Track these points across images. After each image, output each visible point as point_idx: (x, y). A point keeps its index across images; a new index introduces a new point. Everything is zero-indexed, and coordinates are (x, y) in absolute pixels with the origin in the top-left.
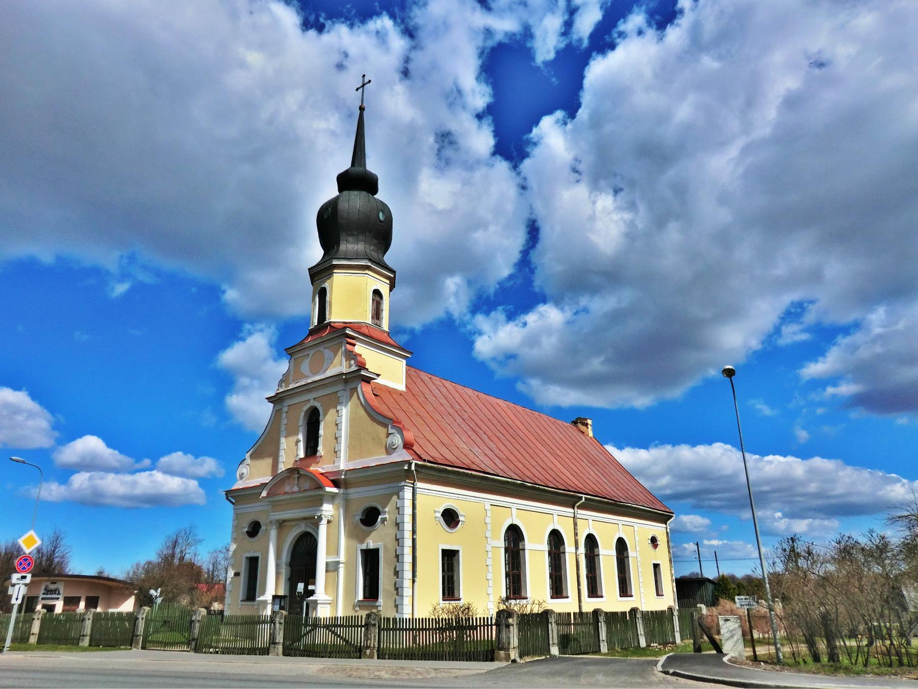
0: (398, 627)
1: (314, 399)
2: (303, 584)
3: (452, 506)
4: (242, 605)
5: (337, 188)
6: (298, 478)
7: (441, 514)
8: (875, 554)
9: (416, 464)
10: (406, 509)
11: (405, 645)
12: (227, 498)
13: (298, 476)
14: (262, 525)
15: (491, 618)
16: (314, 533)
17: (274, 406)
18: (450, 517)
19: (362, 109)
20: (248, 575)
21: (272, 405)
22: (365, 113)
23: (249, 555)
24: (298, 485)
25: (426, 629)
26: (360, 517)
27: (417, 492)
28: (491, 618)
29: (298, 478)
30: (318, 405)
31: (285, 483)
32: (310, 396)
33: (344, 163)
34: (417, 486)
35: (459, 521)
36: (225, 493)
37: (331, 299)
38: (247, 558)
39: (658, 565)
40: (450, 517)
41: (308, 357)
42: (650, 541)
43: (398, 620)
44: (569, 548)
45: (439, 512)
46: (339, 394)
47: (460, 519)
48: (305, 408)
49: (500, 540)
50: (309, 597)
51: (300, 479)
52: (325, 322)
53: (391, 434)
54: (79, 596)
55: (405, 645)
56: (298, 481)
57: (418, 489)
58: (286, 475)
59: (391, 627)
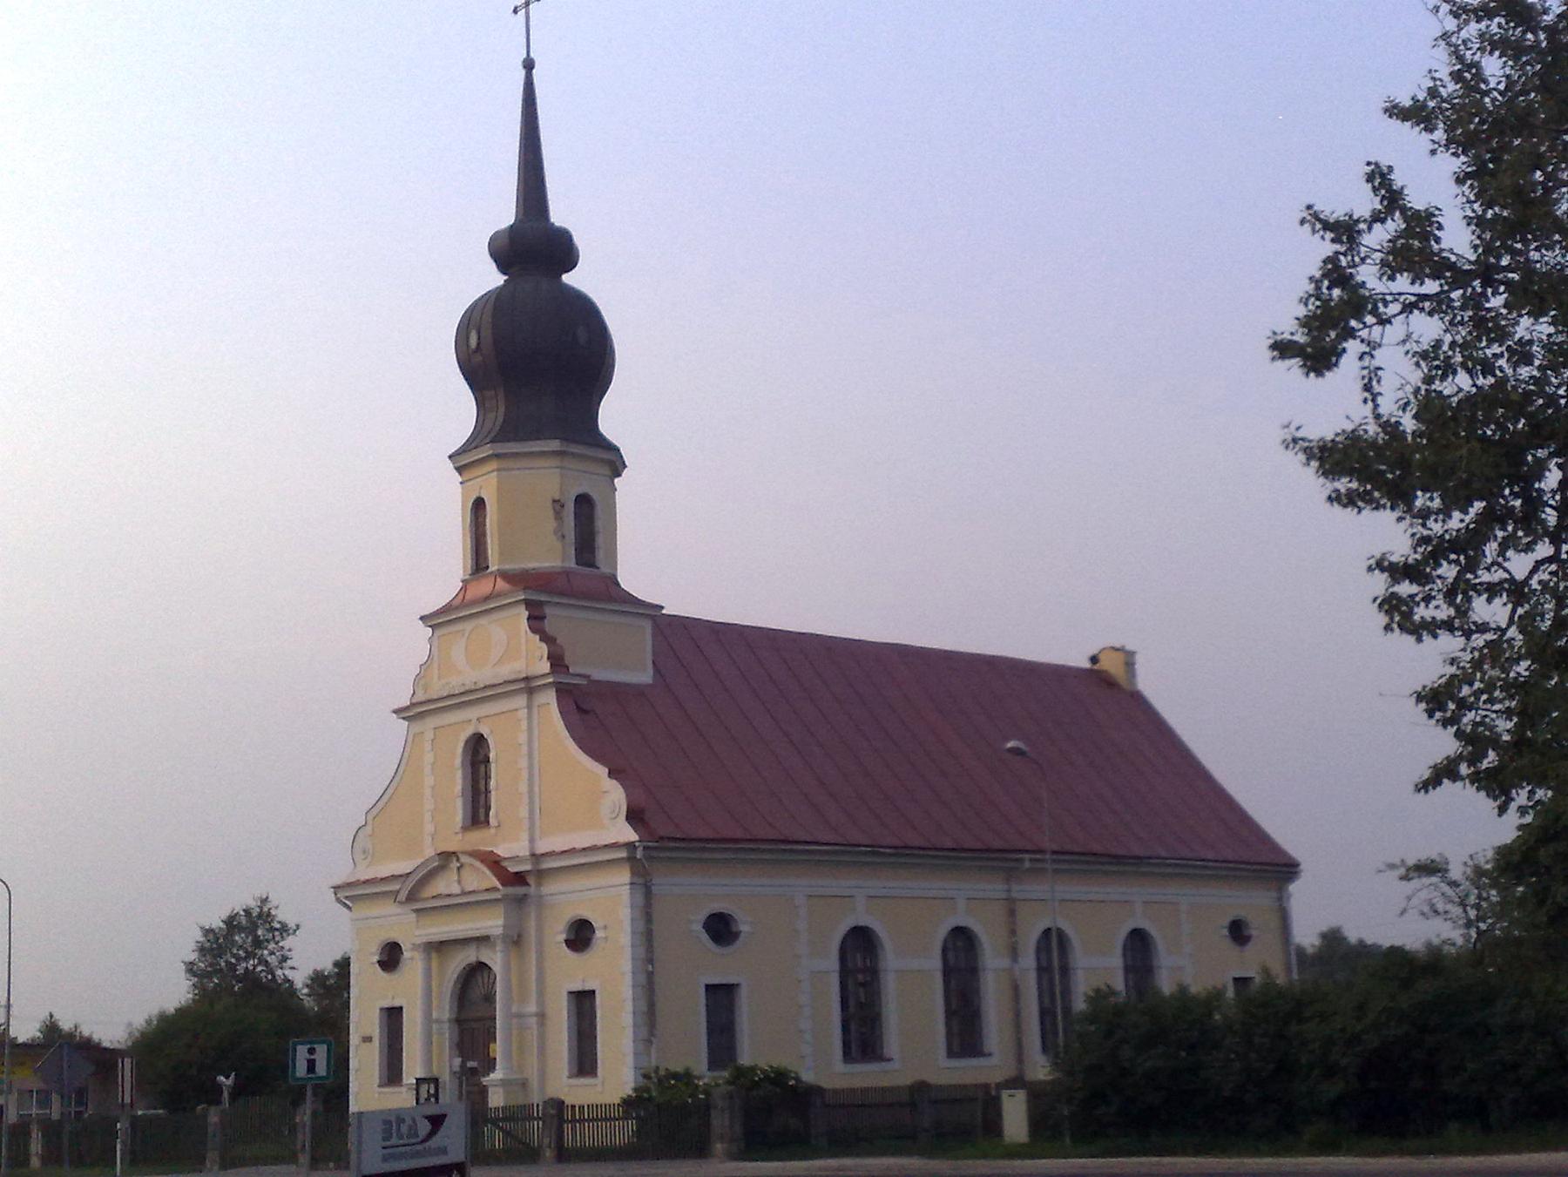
0: (586, 1117)
2: (651, 682)
4: (380, 1093)
6: (459, 869)
12: (338, 900)
13: (458, 865)
14: (403, 948)
15: (538, 1105)
18: (721, 928)
19: (529, 65)
23: (387, 1003)
24: (459, 882)
25: (606, 1119)
26: (564, 936)
28: (538, 1105)
29: (459, 869)
32: (473, 713)
33: (504, 214)
36: (332, 890)
38: (381, 1009)
40: (721, 928)
41: (463, 635)
42: (1226, 932)
43: (535, 1105)
44: (991, 958)
50: (1471, 270)
59: (577, 1117)
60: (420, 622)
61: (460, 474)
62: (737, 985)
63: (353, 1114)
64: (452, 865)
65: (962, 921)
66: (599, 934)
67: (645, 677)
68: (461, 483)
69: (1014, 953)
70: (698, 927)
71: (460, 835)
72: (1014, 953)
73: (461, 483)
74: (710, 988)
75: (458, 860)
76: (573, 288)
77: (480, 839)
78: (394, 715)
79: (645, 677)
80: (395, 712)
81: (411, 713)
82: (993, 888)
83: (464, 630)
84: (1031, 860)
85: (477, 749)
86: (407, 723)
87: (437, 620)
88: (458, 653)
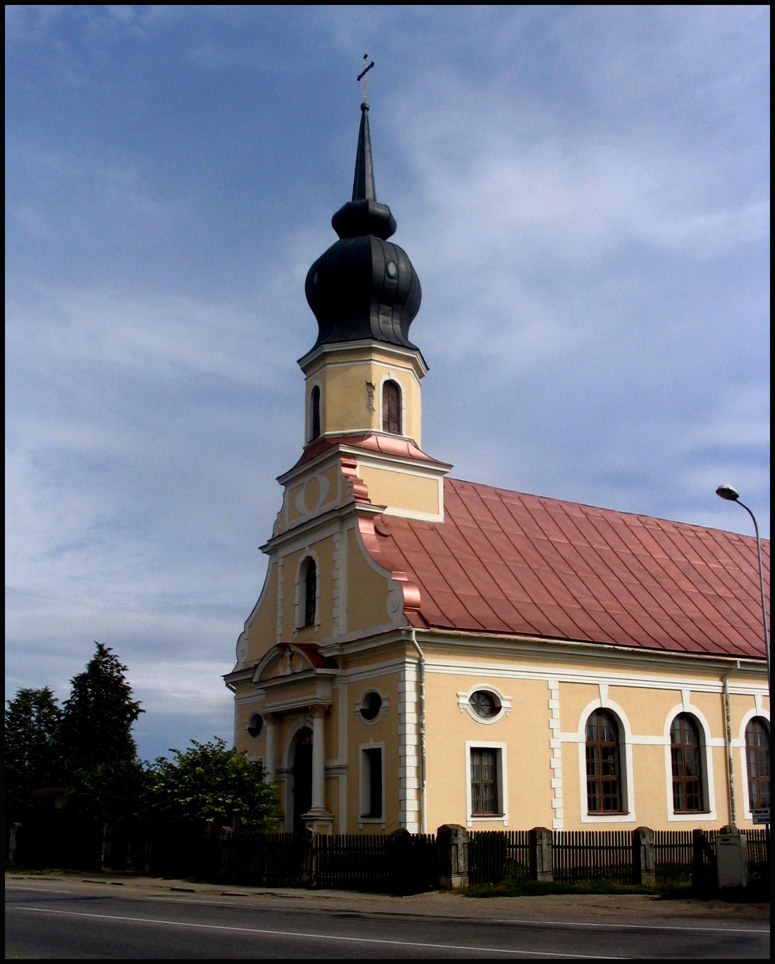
1: (309, 546)
3: (496, 691)
5: (336, 233)
7: (468, 699)
8: (115, 695)
9: (417, 633)
10: (407, 694)
11: (663, 851)
13: (290, 653)
16: (310, 727)
17: (270, 558)
20: (369, 790)
21: (267, 557)
22: (369, 114)
24: (291, 666)
27: (425, 670)
30: (313, 554)
31: (278, 663)
33: (346, 196)
34: (426, 663)
35: (501, 707)
37: (324, 402)
39: (494, 754)
41: (303, 487)
44: (713, 742)
45: (466, 697)
46: (336, 538)
47: (502, 705)
48: (301, 559)
49: (662, 735)
51: (293, 658)
52: (320, 437)
53: (390, 591)
54: (506, 809)
55: (663, 851)
56: (291, 659)
57: (426, 667)
58: (276, 653)
60: (277, 481)
61: (306, 374)
62: (102, 651)
63: (753, 708)
64: (286, 654)
65: (689, 708)
66: (385, 704)
67: (439, 518)
68: (305, 379)
69: (727, 734)
70: (465, 701)
71: (297, 633)
72: (727, 734)
73: (305, 379)
74: (476, 752)
75: (290, 651)
76: (413, 319)
77: (308, 637)
78: (260, 550)
79: (439, 518)
80: (260, 548)
81: (270, 549)
82: (713, 684)
83: (303, 483)
84: (741, 663)
85: (309, 566)
86: (269, 556)
87: (285, 480)
88: (300, 502)
